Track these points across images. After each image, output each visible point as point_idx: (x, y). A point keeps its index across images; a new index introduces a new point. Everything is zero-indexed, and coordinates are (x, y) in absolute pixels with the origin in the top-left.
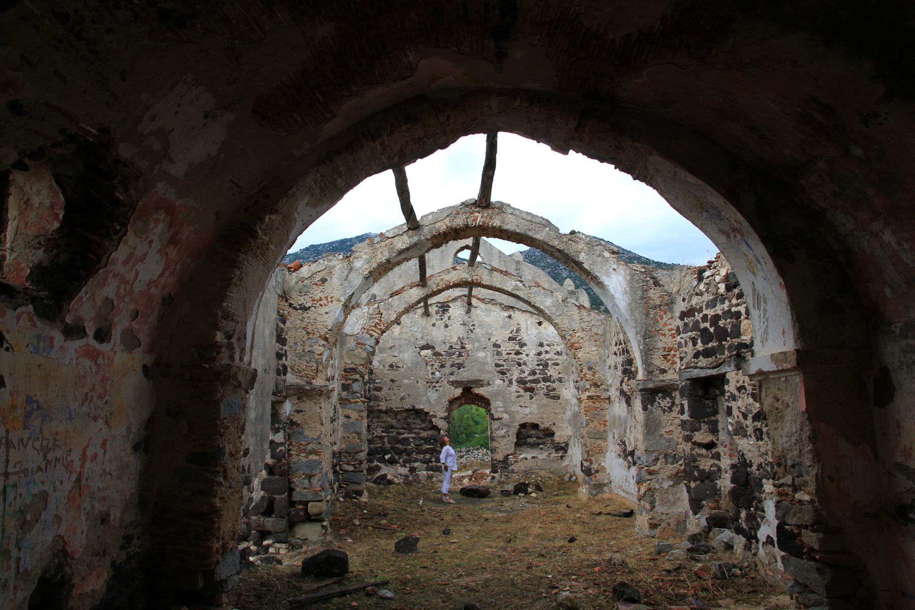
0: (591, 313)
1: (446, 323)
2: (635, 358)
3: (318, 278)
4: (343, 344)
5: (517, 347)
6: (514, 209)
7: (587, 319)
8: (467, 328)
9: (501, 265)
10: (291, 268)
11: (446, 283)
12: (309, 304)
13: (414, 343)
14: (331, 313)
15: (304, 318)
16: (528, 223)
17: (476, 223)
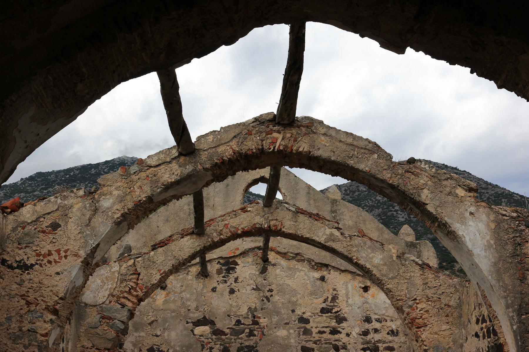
0: (440, 275)
1: (232, 286)
2: (506, 343)
3: (46, 223)
4: (80, 317)
5: (333, 323)
6: (328, 127)
7: (433, 283)
8: (262, 294)
9: (310, 204)
10: (7, 208)
11: (233, 230)
12: (32, 261)
13: (185, 317)
14: (65, 273)
15: (23, 281)
16: (348, 148)
17: (274, 148)
